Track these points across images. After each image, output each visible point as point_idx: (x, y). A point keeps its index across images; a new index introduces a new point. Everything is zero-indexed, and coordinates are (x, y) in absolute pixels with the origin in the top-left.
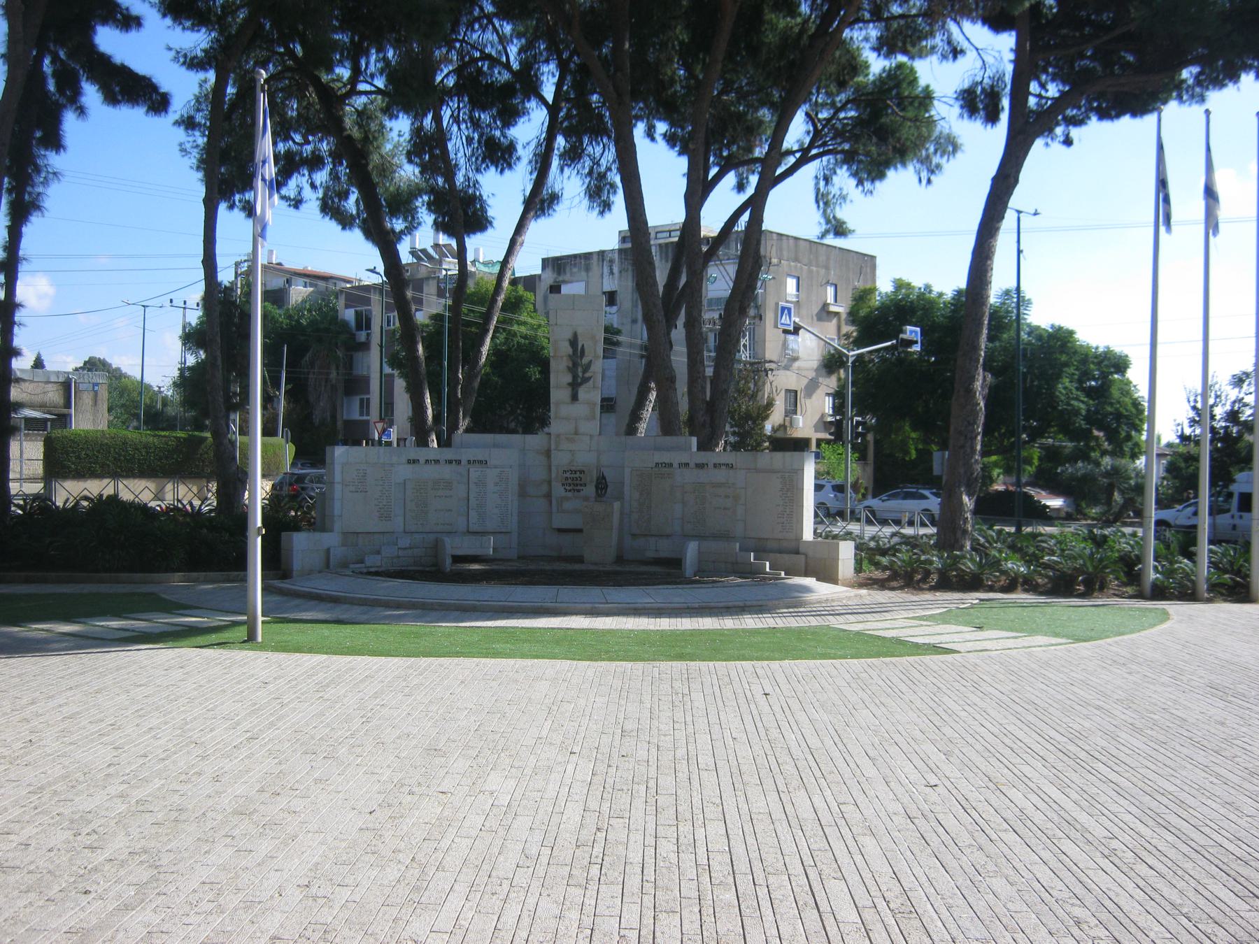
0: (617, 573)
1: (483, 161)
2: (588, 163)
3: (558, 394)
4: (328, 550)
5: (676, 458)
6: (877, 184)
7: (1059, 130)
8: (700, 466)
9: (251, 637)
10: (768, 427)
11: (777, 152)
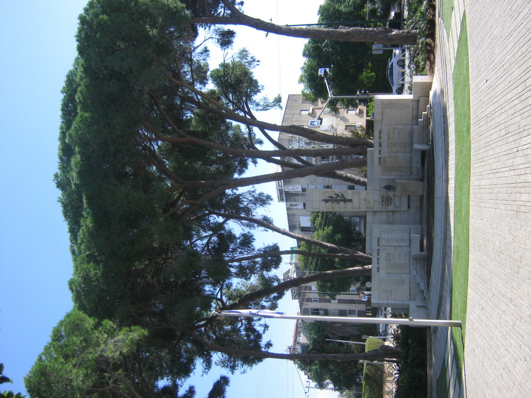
0: (428, 179)
1: (250, 247)
2: (251, 205)
4: (417, 306)
5: (377, 156)
6: (259, 84)
8: (380, 145)
9: (459, 325)
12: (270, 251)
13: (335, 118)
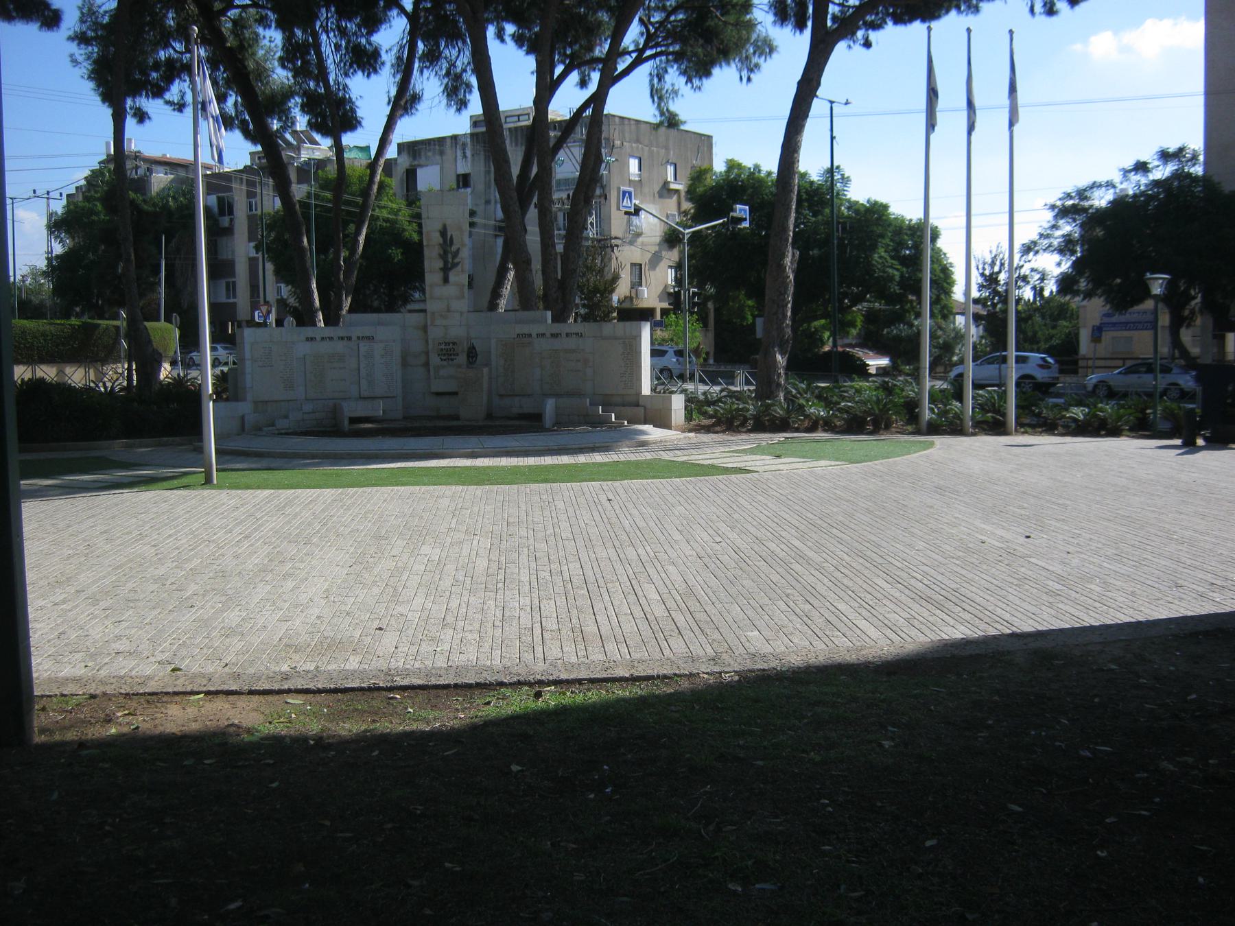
1: (351, 66)
2: (445, 65)
3: (432, 277)
4: (243, 418)
5: (535, 330)
6: (704, 80)
7: (860, 34)
8: (555, 336)
9: (208, 481)
10: (615, 298)
11: (616, 52)
12: (346, 111)
13: (658, 240)
